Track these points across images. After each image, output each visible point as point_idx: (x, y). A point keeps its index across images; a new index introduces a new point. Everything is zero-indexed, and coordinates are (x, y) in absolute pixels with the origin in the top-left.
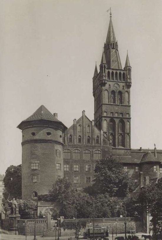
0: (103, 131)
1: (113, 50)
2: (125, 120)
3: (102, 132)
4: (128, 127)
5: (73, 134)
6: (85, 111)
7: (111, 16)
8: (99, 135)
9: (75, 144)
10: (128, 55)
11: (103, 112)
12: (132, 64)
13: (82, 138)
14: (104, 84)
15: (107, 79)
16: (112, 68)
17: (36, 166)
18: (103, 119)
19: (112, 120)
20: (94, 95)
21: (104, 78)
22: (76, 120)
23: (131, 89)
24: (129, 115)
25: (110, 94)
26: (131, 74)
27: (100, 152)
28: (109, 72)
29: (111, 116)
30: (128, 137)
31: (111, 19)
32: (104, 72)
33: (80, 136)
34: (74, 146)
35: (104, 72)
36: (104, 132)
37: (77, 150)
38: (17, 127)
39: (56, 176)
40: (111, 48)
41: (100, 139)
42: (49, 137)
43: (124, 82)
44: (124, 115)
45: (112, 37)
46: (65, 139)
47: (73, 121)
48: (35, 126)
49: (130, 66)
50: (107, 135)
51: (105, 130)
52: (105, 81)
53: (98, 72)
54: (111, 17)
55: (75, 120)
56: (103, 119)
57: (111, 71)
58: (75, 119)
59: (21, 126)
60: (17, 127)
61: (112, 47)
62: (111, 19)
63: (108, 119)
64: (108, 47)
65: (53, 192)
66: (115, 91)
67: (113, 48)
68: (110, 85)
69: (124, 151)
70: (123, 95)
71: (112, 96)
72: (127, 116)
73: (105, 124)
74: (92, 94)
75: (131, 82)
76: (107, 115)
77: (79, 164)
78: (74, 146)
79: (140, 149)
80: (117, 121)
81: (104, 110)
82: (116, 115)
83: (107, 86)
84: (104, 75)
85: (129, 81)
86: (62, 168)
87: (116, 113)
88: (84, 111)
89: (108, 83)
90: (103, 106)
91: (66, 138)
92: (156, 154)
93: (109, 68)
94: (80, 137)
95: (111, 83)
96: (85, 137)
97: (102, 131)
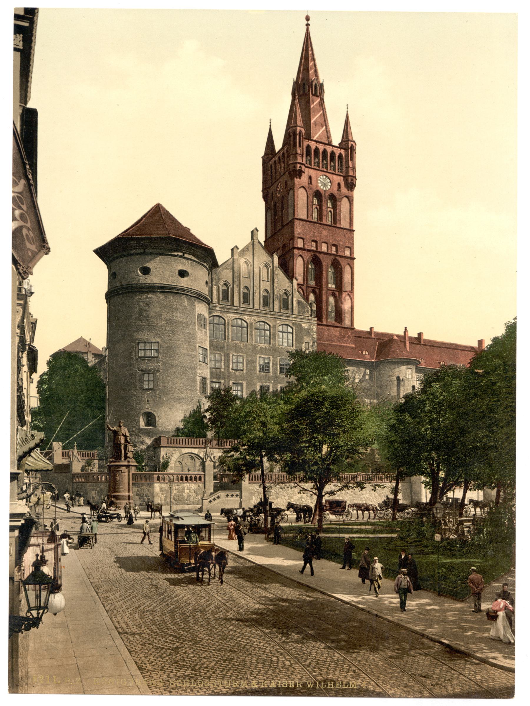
0: (297, 280)
1: (314, 97)
2: (342, 261)
3: (295, 282)
4: (347, 277)
5: (230, 281)
6: (258, 231)
7: (309, 22)
8: (289, 289)
9: (235, 304)
10: (349, 113)
11: (295, 239)
12: (356, 134)
13: (251, 293)
14: (299, 174)
15: (304, 162)
16: (315, 139)
17: (152, 349)
18: (296, 252)
19: (316, 261)
20: (265, 197)
21: (299, 160)
22: (238, 249)
23: (357, 193)
24: (352, 252)
25: (311, 197)
26: (355, 159)
27: (290, 330)
28: (308, 147)
29: (313, 248)
30: (350, 301)
31: (308, 29)
32: (300, 146)
33: (247, 288)
34: (251, 313)
35: (300, 146)
36: (298, 284)
37: (239, 321)
38: (97, 252)
39: (198, 378)
40: (311, 95)
41: (290, 298)
42: (184, 282)
43: (340, 176)
44: (339, 250)
45: (313, 70)
46: (212, 291)
47: (230, 251)
48: (151, 251)
49: (354, 142)
50: (302, 290)
51: (301, 280)
52: (300, 167)
53: (277, 149)
54: (308, 25)
55: (235, 250)
56: (296, 252)
57: (313, 145)
58: (236, 247)
59: (101, 252)
60: (97, 252)
61: (314, 92)
62: (308, 29)
63: (307, 256)
64: (304, 92)
65: (188, 418)
66: (323, 193)
67: (315, 95)
68: (310, 178)
69: (340, 333)
70: (338, 203)
71: (315, 202)
72: (347, 253)
73: (299, 265)
74: (261, 194)
75: (355, 177)
76: (304, 246)
77: (245, 355)
78: (251, 313)
79: (370, 333)
80: (326, 262)
81: (299, 234)
82: (324, 248)
83: (304, 179)
84: (299, 151)
85: (351, 173)
86: (208, 360)
87: (334, 245)
88: (256, 229)
89: (308, 172)
90: (295, 220)
91: (215, 288)
92: (408, 344)
93: (309, 137)
94: (246, 291)
95: (312, 173)
96: (258, 291)
97: (295, 282)
